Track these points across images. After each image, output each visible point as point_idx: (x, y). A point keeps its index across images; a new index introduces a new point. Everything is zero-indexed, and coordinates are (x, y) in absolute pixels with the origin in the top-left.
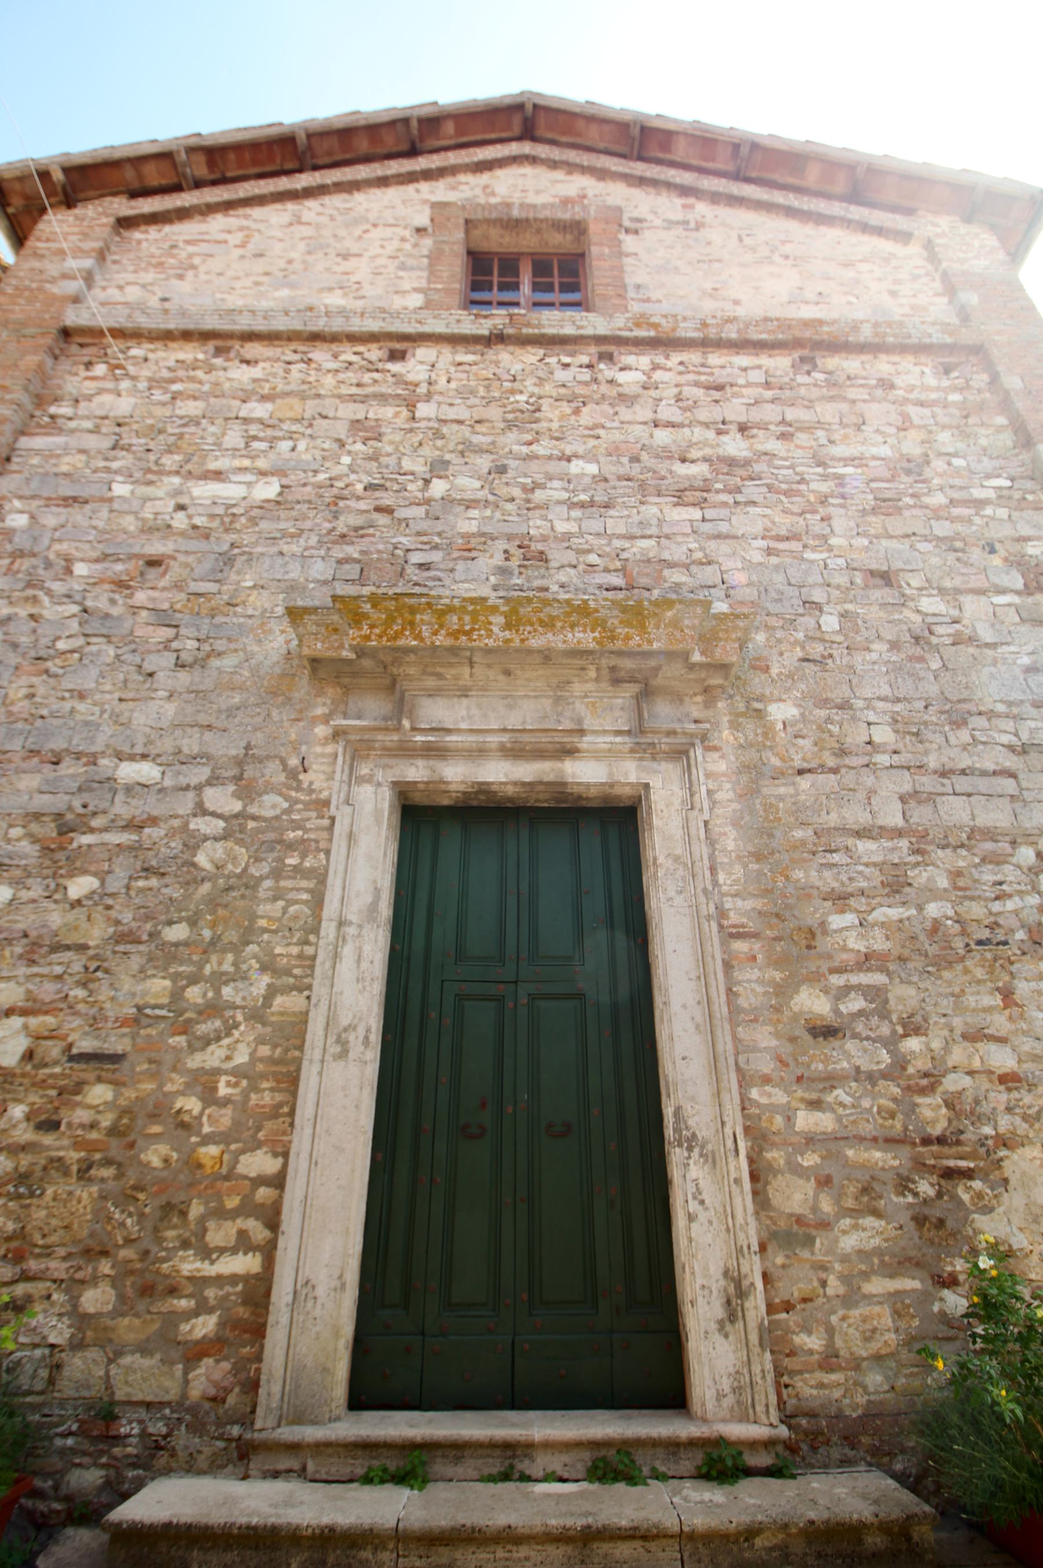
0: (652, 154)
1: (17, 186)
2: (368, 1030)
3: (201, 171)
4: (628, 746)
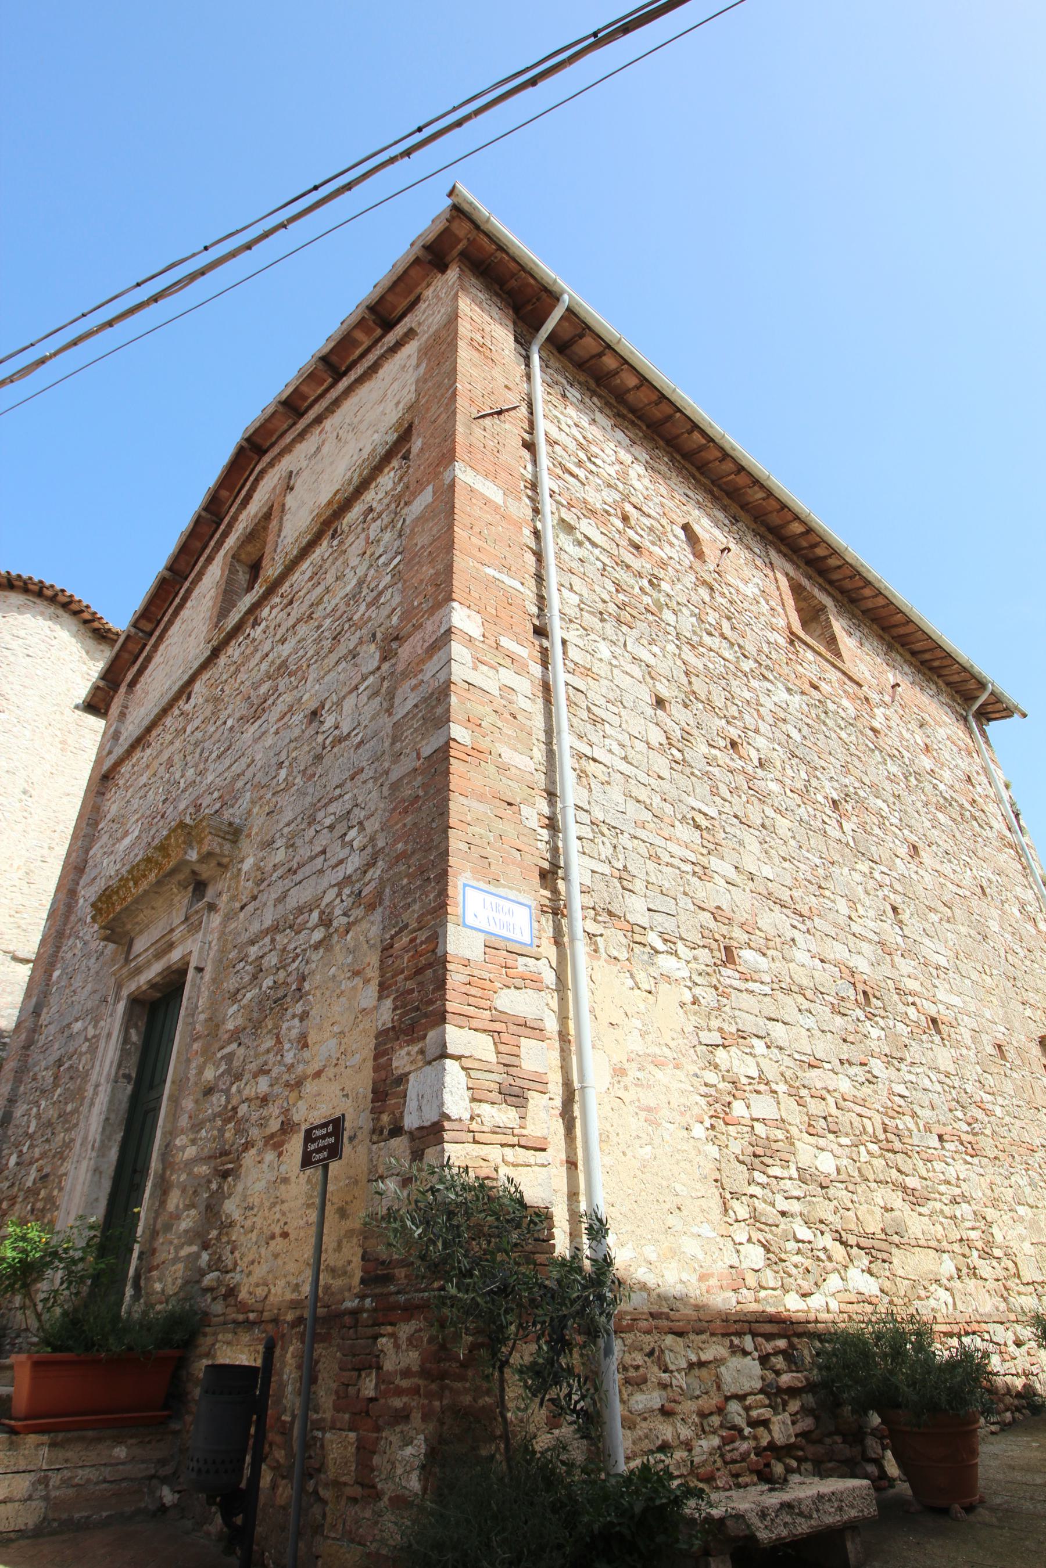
0: (303, 408)
1: (96, 699)
2: (95, 1141)
3: (148, 627)
4: (185, 932)
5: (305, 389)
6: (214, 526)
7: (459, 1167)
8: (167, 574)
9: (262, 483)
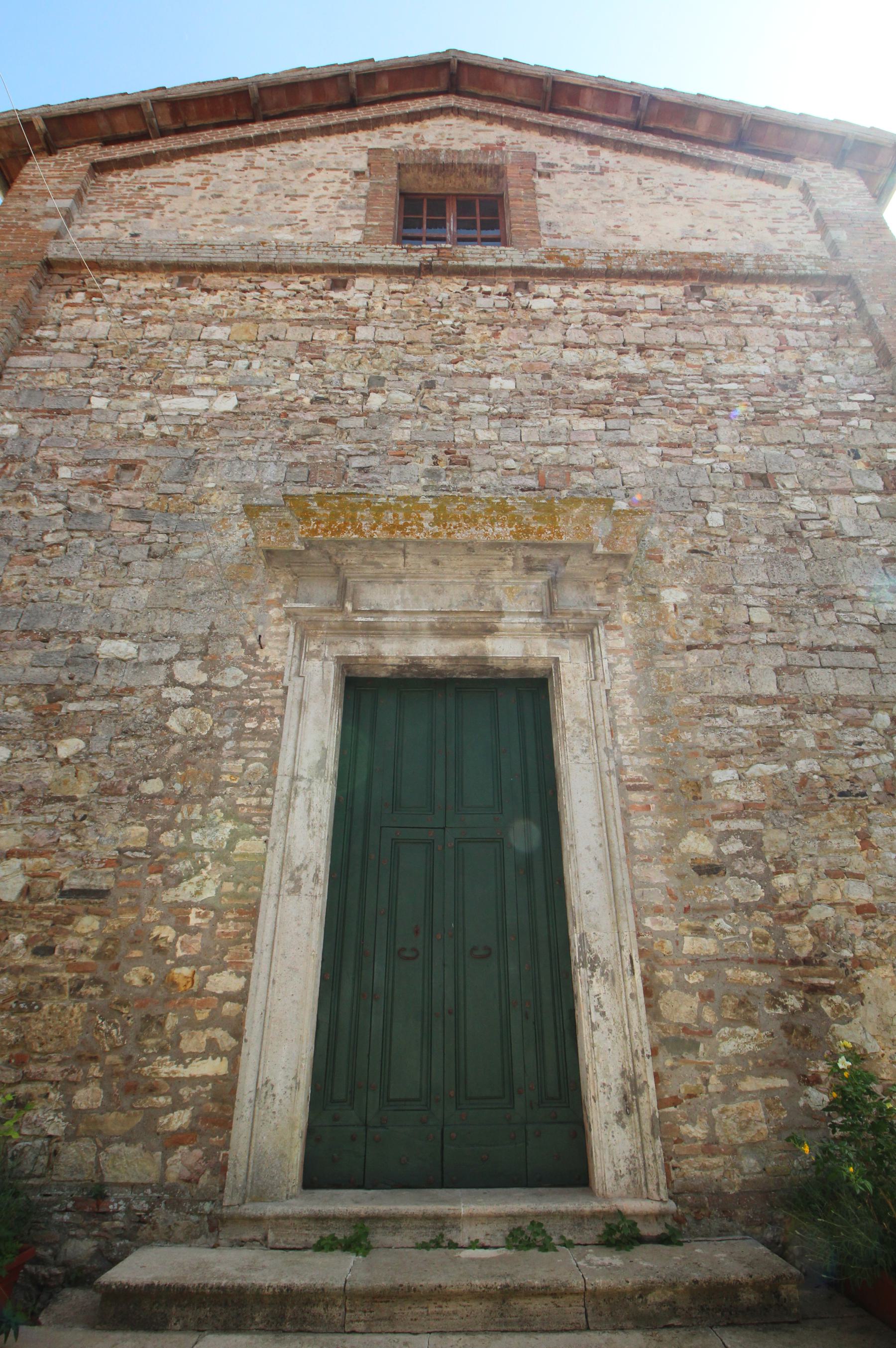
0: (562, 106)
3: (166, 121)
5: (588, 96)
6: (344, 100)
7: (241, 997)
8: (254, 91)
9: (453, 120)
